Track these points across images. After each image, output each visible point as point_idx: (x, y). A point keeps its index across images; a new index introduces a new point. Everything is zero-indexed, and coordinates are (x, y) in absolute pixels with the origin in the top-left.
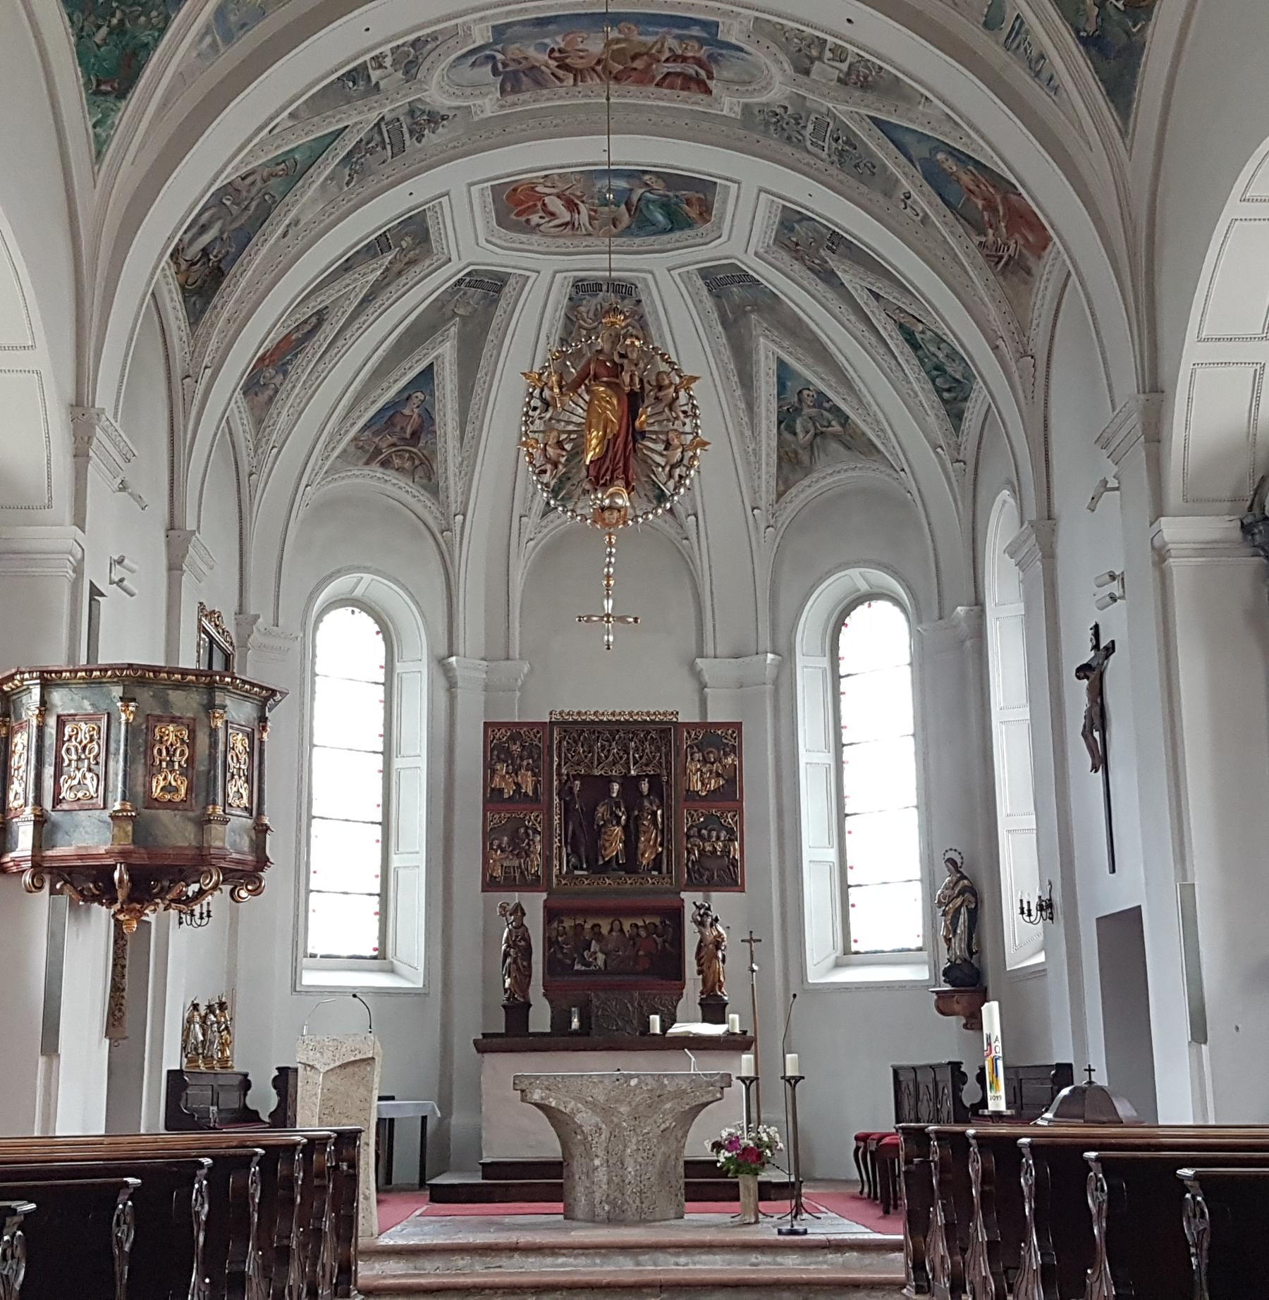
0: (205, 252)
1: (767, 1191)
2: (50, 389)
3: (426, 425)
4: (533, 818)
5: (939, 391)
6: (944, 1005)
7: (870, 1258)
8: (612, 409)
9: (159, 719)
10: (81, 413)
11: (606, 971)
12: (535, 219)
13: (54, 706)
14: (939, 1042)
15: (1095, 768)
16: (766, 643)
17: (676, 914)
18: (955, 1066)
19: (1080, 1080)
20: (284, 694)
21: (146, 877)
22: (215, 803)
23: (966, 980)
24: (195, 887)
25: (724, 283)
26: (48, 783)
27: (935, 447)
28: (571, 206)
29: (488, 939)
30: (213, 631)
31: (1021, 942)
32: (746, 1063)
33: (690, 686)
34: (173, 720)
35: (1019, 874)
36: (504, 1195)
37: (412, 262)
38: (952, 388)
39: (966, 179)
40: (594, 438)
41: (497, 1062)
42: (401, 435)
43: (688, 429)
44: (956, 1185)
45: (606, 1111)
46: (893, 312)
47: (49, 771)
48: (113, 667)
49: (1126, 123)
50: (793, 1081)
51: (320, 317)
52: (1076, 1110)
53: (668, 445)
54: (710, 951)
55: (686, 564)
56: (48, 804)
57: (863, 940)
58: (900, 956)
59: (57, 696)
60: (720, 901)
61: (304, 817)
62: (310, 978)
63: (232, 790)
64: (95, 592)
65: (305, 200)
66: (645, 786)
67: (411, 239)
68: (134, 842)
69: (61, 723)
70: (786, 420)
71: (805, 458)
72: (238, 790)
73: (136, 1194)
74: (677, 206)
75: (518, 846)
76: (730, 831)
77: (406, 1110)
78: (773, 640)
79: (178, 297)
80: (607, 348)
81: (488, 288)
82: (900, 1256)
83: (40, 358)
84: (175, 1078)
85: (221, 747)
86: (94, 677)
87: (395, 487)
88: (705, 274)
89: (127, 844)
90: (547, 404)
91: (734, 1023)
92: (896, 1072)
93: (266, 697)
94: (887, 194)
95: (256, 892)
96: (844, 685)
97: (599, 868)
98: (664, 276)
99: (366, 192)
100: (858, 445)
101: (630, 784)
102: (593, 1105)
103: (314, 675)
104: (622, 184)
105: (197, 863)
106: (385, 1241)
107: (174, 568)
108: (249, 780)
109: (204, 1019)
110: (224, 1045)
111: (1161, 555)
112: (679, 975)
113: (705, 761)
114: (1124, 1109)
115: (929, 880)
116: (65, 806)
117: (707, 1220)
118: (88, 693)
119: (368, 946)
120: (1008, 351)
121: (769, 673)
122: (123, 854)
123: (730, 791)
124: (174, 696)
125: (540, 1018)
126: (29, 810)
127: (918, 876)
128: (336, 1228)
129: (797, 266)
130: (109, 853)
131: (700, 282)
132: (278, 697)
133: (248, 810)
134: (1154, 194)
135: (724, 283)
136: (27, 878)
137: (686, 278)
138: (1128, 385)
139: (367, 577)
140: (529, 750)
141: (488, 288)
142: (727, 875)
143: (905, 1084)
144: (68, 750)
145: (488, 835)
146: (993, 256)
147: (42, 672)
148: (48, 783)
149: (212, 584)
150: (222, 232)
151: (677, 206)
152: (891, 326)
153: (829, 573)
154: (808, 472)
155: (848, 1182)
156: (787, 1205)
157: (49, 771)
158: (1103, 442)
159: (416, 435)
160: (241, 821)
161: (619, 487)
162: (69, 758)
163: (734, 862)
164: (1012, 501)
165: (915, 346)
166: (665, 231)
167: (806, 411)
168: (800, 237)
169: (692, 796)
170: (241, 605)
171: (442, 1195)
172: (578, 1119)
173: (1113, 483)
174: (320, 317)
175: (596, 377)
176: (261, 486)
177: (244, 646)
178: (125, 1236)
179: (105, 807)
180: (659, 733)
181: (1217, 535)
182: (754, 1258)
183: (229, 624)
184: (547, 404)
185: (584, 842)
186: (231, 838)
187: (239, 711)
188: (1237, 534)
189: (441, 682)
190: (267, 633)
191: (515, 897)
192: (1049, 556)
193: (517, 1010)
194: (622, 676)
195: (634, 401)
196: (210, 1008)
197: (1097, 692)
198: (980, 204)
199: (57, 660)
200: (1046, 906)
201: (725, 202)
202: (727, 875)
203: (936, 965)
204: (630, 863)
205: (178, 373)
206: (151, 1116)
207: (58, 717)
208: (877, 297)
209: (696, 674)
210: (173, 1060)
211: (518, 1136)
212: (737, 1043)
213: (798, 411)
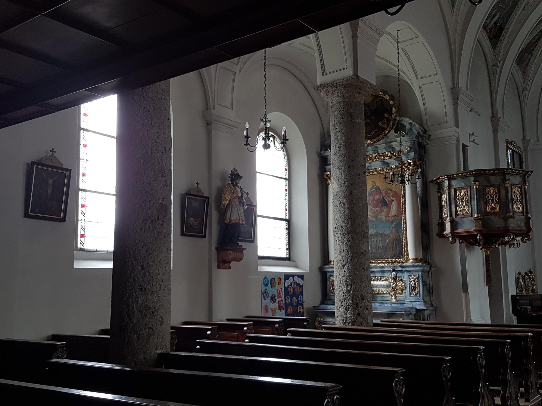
0: (495, 23)
9: (487, 186)
10: (454, 91)
13: (453, 185)
20: (532, 172)
22: (509, 212)
30: (513, 148)
34: (492, 186)
47: (453, 206)
56: (454, 216)
59: (453, 183)
63: (515, 206)
68: (483, 226)
69: (455, 191)
72: (518, 207)
79: (488, 41)
85: (510, 193)
105: (506, 231)
107: (495, 131)
108: (521, 203)
109: (524, 278)
110: (533, 285)
116: (459, 216)
118: (463, 180)
122: (479, 231)
124: (492, 178)
126: (448, 218)
132: (530, 173)
133: (522, 213)
136: (450, 239)
144: (458, 199)
147: (447, 176)
149: (511, 130)
150: (501, 15)
170: (524, 137)
176: (527, 94)
177: (526, 150)
179: (472, 216)
186: (516, 223)
196: (526, 274)
199: (453, 171)
205: (490, 64)
206: (509, 317)
207: (454, 189)
210: (513, 291)
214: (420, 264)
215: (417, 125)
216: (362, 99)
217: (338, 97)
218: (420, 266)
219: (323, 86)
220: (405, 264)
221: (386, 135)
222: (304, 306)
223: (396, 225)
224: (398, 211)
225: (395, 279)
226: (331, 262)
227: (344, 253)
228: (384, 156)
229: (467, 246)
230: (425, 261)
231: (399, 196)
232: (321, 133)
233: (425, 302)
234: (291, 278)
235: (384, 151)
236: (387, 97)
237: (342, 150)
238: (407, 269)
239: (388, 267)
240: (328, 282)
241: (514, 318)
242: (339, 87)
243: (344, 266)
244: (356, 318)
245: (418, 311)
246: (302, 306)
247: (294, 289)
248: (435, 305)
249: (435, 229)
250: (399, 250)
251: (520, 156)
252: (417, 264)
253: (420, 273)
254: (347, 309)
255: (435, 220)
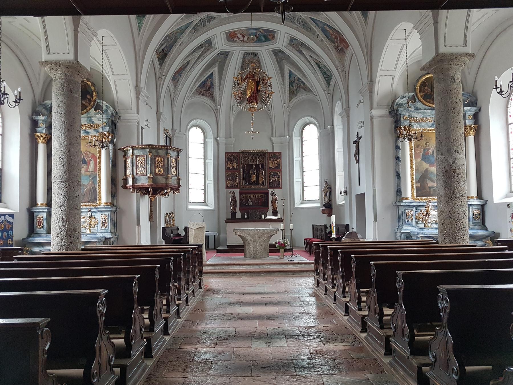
0: (163, 50)
1: (286, 251)
2: (130, 82)
3: (212, 86)
4: (236, 173)
5: (325, 78)
6: (323, 212)
7: (306, 266)
8: (253, 85)
9: (157, 156)
10: (137, 88)
11: (252, 206)
12: (235, 39)
14: (322, 220)
15: (357, 163)
16: (287, 134)
17: (267, 194)
18: (325, 225)
19: (351, 230)
21: (156, 190)
23: (328, 207)
24: (166, 191)
25: (278, 54)
26: (135, 170)
27: (324, 90)
28: (243, 36)
29: (227, 198)
31: (340, 199)
32: (282, 226)
33: (270, 143)
34: (160, 156)
35: (340, 185)
36: (232, 252)
37: (208, 50)
38: (328, 77)
39: (331, 32)
40: (249, 92)
41: (229, 224)
42: (206, 89)
43: (270, 89)
44: (325, 256)
45: (253, 236)
46: (314, 60)
47: (135, 167)
48: (147, 145)
49: (366, 20)
50: (292, 230)
51: (188, 63)
52: (350, 237)
53: (265, 93)
54: (274, 201)
55: (269, 117)
56: (135, 174)
57: (307, 198)
58: (314, 201)
59: (135, 151)
60: (276, 191)
61: (187, 173)
62: (190, 207)
63: (172, 171)
64: (142, 128)
65: (185, 37)
66: (260, 166)
67: (208, 44)
69: (136, 157)
70: (291, 84)
71: (295, 92)
72: (174, 171)
73: (159, 268)
74: (267, 36)
75: (233, 180)
76: (279, 176)
77: (211, 234)
78: (288, 133)
79: (157, 60)
80: (252, 71)
81: (225, 55)
82: (313, 265)
83: (128, 77)
84: (164, 228)
86: (143, 147)
87: (205, 100)
88: (273, 51)
89: (151, 183)
90: (238, 84)
91: (279, 216)
92: (313, 226)
93: (179, 151)
94: (314, 34)
95: (178, 192)
96: (304, 143)
97: (251, 184)
98: (264, 52)
99: (198, 35)
100: (307, 89)
101: (256, 165)
102: (250, 235)
103: (189, 142)
104: (255, 31)
105: (166, 186)
106: (208, 263)
107: (158, 121)
109: (169, 216)
110: (173, 221)
111: (372, 118)
112: (268, 206)
113: (273, 161)
114: (359, 236)
115: (321, 185)
117: (274, 257)
119: (202, 200)
120: (340, 70)
121: (287, 140)
123: (279, 167)
124: (160, 151)
125: (239, 215)
127: (319, 184)
128: (198, 265)
129: (294, 49)
130: (148, 185)
131: (272, 53)
134: (372, 36)
135: (278, 54)
136: (131, 190)
137: (269, 52)
138: (366, 80)
139: (199, 120)
140: (235, 159)
141: (225, 55)
142: (278, 185)
143: (315, 228)
145: (227, 177)
146: (337, 49)
148: (135, 170)
149: (166, 123)
151: (267, 36)
152: (314, 63)
153: (300, 118)
154: (296, 95)
155: (303, 247)
156: (290, 253)
157: (135, 167)
158: (360, 92)
159: (209, 88)
160: (174, 178)
161: (254, 103)
162: (139, 165)
163: (279, 182)
164: (340, 103)
165: (320, 68)
166: (264, 42)
167: (296, 82)
168: (294, 43)
169: (270, 168)
171: (219, 251)
172: (247, 238)
173: (362, 101)
174: (188, 63)
175: (249, 78)
177: (173, 136)
178: (157, 277)
180: (263, 154)
181: (383, 113)
182: (283, 266)
183: (170, 132)
184: (238, 84)
185: (247, 178)
186: (173, 181)
187: (173, 154)
188: (388, 113)
189: (216, 143)
190: (178, 133)
191: (233, 190)
192: (348, 116)
193: (234, 214)
194: (256, 142)
195: (258, 83)
196: (170, 214)
197: (358, 147)
198: (334, 37)
199: (135, 144)
200: (345, 192)
201: (277, 35)
202: (278, 185)
203: (322, 203)
204: (257, 183)
205: (158, 77)
206: (160, 241)
208: (311, 57)
209: (271, 141)
210: (163, 225)
211: (234, 240)
212: (280, 220)
213: (294, 82)
214: (110, 207)
215: (111, 108)
216: (79, 79)
217: (61, 74)
218: (110, 208)
219: (47, 63)
220: (99, 207)
221: (88, 111)
222: (13, 239)
223: (93, 178)
224: (95, 168)
225: (90, 217)
226: (38, 204)
227: (62, 197)
228: (86, 127)
229: (141, 195)
230: (113, 205)
231: (96, 157)
232: (32, 100)
233: (111, 233)
234: (3, 217)
235: (86, 123)
236: (89, 83)
237: (63, 116)
238: (100, 210)
239: (85, 209)
240: (35, 220)
241: (164, 241)
242: (61, 66)
243: (61, 206)
244: (69, 245)
245: (106, 239)
246: (12, 239)
247: (5, 225)
248: (117, 234)
249: (121, 183)
250: (94, 196)
251: (170, 139)
252: (107, 207)
253: (109, 213)
254: (62, 239)
255: (121, 176)
